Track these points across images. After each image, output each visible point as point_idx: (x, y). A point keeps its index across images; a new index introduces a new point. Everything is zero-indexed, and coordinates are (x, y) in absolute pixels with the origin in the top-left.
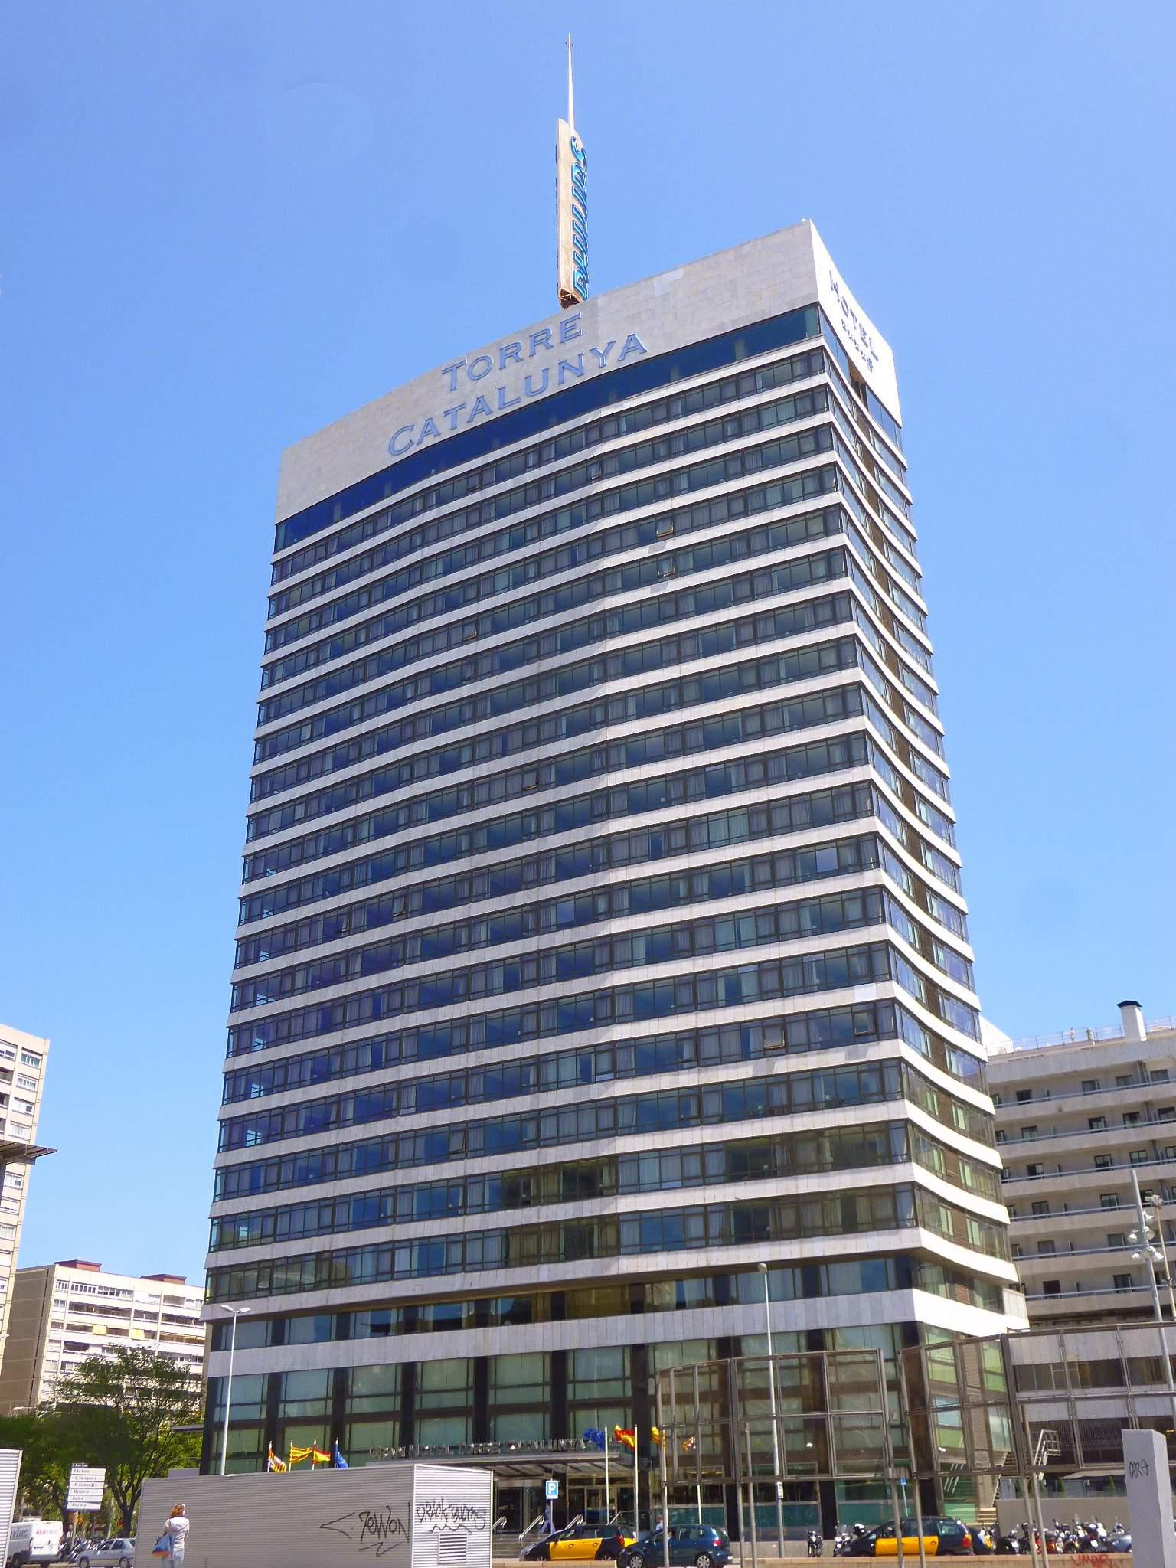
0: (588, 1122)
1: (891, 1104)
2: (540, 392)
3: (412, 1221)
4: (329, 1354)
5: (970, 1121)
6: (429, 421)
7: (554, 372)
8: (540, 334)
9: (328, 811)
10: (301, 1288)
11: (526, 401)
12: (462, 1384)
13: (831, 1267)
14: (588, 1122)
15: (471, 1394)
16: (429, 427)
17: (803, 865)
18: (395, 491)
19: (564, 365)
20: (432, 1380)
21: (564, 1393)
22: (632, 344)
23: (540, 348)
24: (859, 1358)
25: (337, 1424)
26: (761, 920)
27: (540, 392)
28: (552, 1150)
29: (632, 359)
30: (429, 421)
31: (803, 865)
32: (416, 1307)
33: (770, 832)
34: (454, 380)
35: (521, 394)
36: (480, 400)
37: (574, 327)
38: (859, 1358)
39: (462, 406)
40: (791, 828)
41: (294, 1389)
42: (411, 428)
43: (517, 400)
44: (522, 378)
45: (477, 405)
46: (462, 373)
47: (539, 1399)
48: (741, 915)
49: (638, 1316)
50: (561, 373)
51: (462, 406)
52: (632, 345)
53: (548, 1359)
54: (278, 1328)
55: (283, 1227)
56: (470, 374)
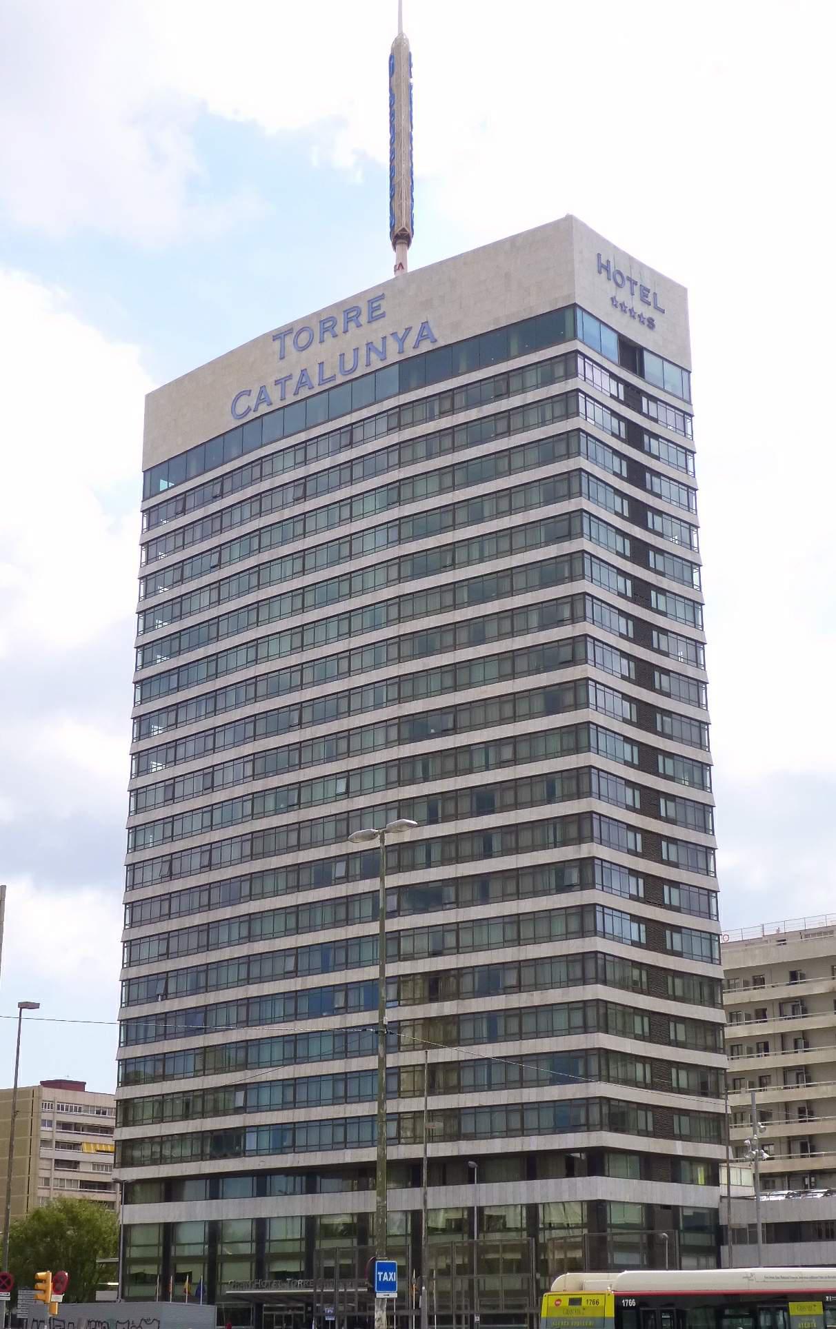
2: (353, 370)
3: (414, 1096)
4: (303, 1205)
6: (263, 390)
7: (363, 352)
8: (328, 320)
9: (538, 671)
10: (182, 1160)
12: (156, 1242)
13: (227, 1180)
15: (304, 1243)
19: (370, 346)
20: (616, 1217)
21: (264, 1247)
23: (327, 335)
27: (353, 370)
28: (354, 1061)
29: (426, 347)
30: (263, 390)
34: (283, 348)
35: (337, 371)
36: (304, 372)
37: (379, 307)
39: (290, 377)
41: (185, 1235)
42: (249, 393)
43: (333, 378)
45: (301, 378)
46: (289, 341)
47: (297, 1250)
50: (368, 356)
51: (290, 377)
52: (425, 332)
53: (585, 1206)
54: (170, 1189)
56: (295, 343)
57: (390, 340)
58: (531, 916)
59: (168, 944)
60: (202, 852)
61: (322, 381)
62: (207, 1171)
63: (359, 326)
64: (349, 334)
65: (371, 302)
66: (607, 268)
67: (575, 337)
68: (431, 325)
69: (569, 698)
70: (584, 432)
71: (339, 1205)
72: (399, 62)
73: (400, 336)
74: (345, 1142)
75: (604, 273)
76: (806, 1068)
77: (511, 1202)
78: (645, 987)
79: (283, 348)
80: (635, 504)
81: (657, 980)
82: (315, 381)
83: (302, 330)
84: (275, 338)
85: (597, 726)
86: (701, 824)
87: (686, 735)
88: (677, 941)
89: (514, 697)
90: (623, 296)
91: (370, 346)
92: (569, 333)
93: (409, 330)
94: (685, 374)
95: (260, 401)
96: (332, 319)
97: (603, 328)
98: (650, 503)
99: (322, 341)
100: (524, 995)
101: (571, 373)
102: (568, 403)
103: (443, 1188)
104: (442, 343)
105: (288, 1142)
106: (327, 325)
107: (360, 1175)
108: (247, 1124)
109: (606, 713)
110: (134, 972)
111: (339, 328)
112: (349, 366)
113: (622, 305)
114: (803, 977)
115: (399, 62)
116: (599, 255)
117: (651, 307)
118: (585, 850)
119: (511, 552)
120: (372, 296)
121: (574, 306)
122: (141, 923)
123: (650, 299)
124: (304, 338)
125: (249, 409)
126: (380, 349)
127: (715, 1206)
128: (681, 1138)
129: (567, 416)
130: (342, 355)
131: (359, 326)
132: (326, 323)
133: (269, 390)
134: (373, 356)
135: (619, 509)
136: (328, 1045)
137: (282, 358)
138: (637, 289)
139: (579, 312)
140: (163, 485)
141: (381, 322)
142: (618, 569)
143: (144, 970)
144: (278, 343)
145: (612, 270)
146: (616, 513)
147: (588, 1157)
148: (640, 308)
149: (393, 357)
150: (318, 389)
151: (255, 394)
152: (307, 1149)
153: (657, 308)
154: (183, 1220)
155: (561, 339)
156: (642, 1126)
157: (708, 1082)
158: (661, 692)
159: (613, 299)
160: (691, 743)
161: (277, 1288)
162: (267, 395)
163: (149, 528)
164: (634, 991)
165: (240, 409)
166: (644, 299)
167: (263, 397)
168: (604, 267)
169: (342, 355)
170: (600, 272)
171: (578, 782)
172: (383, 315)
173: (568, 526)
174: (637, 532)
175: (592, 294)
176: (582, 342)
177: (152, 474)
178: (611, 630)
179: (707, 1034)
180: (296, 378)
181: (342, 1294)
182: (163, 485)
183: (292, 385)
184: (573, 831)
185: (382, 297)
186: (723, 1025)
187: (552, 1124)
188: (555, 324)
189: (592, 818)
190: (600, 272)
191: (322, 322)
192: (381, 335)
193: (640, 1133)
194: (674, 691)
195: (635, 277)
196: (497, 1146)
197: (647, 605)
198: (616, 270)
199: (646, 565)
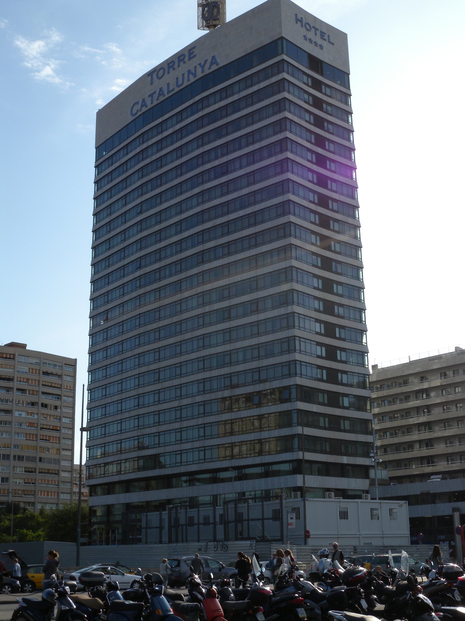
2: (182, 84)
5: (314, 101)
6: (144, 100)
7: (186, 75)
11: (177, 90)
16: (144, 104)
18: (214, 86)
19: (189, 72)
24: (295, 537)
29: (214, 68)
30: (144, 100)
32: (239, 399)
34: (152, 79)
36: (161, 89)
37: (193, 53)
38: (295, 537)
39: (155, 93)
42: (137, 103)
43: (173, 90)
46: (155, 75)
51: (155, 93)
56: (157, 76)
63: (184, 63)
64: (180, 67)
65: (190, 50)
66: (301, 21)
73: (202, 64)
76: (432, 457)
79: (152, 79)
80: (317, 117)
82: (166, 92)
83: (160, 69)
90: (311, 35)
91: (189, 72)
92: (280, 51)
93: (206, 61)
95: (142, 106)
97: (298, 49)
98: (334, 258)
99: (168, 73)
101: (291, 350)
102: (289, 320)
104: (221, 65)
106: (171, 65)
111: (176, 66)
112: (180, 83)
114: (426, 379)
116: (296, 15)
117: (327, 42)
118: (289, 309)
119: (253, 123)
120: (189, 48)
121: (282, 38)
123: (326, 37)
124: (161, 72)
125: (138, 111)
126: (194, 72)
129: (288, 328)
130: (177, 78)
133: (146, 100)
134: (191, 76)
137: (152, 84)
138: (318, 33)
141: (194, 59)
144: (150, 97)
145: (304, 22)
148: (320, 41)
149: (200, 75)
150: (167, 96)
153: (329, 42)
158: (339, 316)
159: (305, 37)
165: (134, 112)
167: (144, 104)
169: (177, 78)
170: (297, 23)
174: (319, 150)
178: (309, 308)
180: (157, 93)
183: (156, 96)
185: (194, 47)
188: (276, 46)
190: (297, 23)
191: (169, 64)
192: (194, 65)
193: (320, 404)
195: (317, 27)
199: (332, 292)
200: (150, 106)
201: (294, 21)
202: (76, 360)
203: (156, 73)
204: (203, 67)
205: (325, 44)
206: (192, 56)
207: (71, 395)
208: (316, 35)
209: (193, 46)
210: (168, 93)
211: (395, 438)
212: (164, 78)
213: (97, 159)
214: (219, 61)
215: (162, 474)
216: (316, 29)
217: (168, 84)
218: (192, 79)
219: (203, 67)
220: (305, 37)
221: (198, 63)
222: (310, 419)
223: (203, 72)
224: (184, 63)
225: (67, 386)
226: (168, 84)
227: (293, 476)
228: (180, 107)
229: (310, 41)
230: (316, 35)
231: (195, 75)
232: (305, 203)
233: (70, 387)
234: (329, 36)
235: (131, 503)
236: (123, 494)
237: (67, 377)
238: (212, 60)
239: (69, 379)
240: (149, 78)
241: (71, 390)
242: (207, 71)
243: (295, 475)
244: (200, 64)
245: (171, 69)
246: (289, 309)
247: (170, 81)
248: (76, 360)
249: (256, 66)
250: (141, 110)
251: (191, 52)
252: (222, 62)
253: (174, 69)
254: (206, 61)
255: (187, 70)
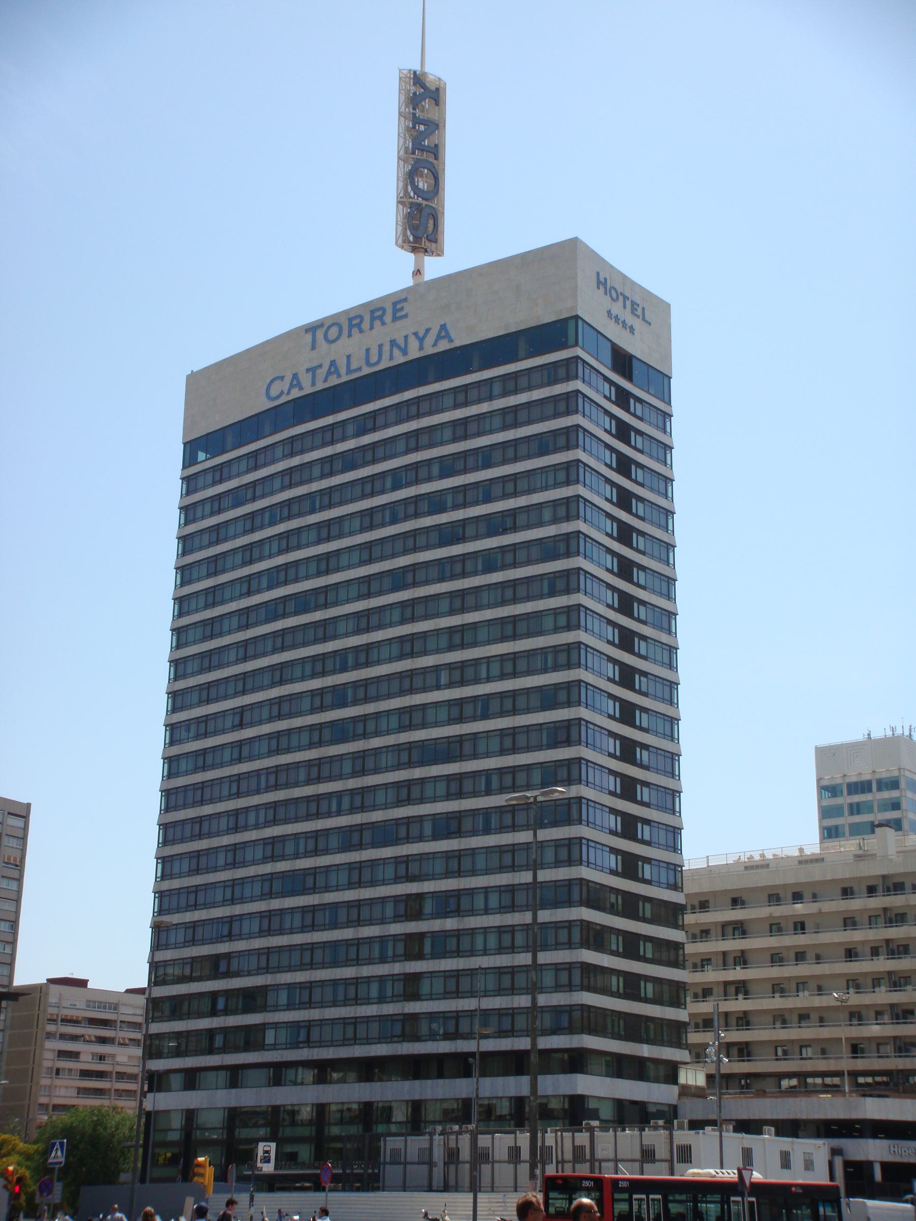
0: (399, 545)
1: (574, 868)
2: (377, 363)
6: (295, 376)
7: (387, 348)
8: (355, 317)
11: (366, 371)
14: (399, 545)
17: (532, 624)
19: (393, 343)
22: (443, 334)
25: (235, 1156)
26: (503, 894)
29: (444, 346)
30: (295, 376)
31: (532, 624)
33: (514, 750)
35: (363, 363)
36: (333, 363)
37: (402, 309)
39: (320, 366)
40: (529, 562)
43: (359, 369)
44: (365, 348)
48: (491, 1012)
49: (417, 1081)
51: (320, 366)
55: (211, 728)
57: (412, 339)
58: (525, 729)
59: (198, 862)
60: (234, 714)
61: (349, 371)
62: (229, 1063)
64: (374, 331)
67: (576, 344)
68: (449, 327)
69: (562, 696)
70: (581, 427)
71: (349, 1093)
72: (423, 101)
73: (421, 335)
74: (355, 1038)
75: (601, 287)
77: (500, 1095)
78: (620, 908)
81: (630, 906)
82: (343, 370)
84: (307, 331)
85: (588, 800)
86: (670, 770)
87: (657, 588)
88: (643, 647)
89: (516, 442)
90: (617, 309)
91: (393, 343)
92: (571, 340)
93: (428, 331)
94: (666, 379)
95: (292, 386)
96: (361, 317)
99: (350, 335)
100: (517, 914)
103: (441, 1081)
104: (458, 343)
105: (302, 1037)
107: (368, 1069)
108: (267, 1021)
109: (598, 755)
110: (166, 885)
111: (366, 325)
113: (616, 318)
115: (423, 101)
116: (598, 274)
118: (574, 791)
121: (577, 318)
122: (176, 808)
123: (639, 312)
125: (282, 393)
126: (403, 346)
127: (675, 1103)
128: (648, 1041)
130: (368, 350)
131: (383, 324)
132: (353, 321)
134: (396, 352)
135: (608, 427)
136: (356, 523)
138: (628, 303)
139: (580, 323)
140: (201, 456)
142: (609, 731)
143: (176, 884)
144: (310, 374)
145: (608, 287)
146: (607, 499)
147: (570, 1057)
148: (630, 320)
149: (414, 353)
150: (345, 378)
151: (288, 380)
152: (321, 1044)
153: (644, 319)
154: (204, 1106)
155: (564, 346)
156: (614, 947)
157: (674, 994)
159: (609, 312)
160: (661, 594)
161: (290, 1168)
162: (299, 382)
163: (186, 524)
164: (611, 913)
165: (274, 392)
166: (633, 311)
168: (601, 283)
169: (368, 350)
170: (598, 288)
171: (569, 656)
172: (406, 316)
173: (565, 734)
175: (593, 309)
176: (583, 349)
177: (191, 448)
179: (670, 953)
181: (349, 1174)
182: (201, 456)
184: (562, 406)
185: (405, 300)
186: (683, 944)
187: (539, 704)
188: (557, 333)
189: (578, 537)
190: (598, 288)
191: (350, 320)
192: (405, 333)
194: (649, 585)
195: (627, 294)
196: (490, 1045)
197: (629, 579)
198: (611, 284)
200: (308, 390)
201: (595, 284)
202: (29, 805)
203: (325, 328)
204: (421, 340)
205: (637, 323)
206: (399, 315)
207: (15, 874)
208: (625, 307)
209: (403, 297)
210: (347, 374)
211: (701, 1004)
212: (339, 342)
213: (187, 463)
214: (453, 335)
215: (315, 1057)
216: (626, 298)
217: (349, 357)
218: (400, 359)
219: (421, 340)
220: (609, 312)
221: (413, 330)
222: (591, 977)
223: (421, 348)
224: (383, 324)
225: (9, 858)
226: (349, 357)
227: (569, 1075)
228: (372, 404)
229: (617, 319)
230: (625, 307)
231: (405, 352)
232: (601, 609)
233: (15, 859)
234: (643, 309)
235: (241, 1108)
236: (225, 1091)
237: (11, 839)
238: (440, 332)
239: (13, 843)
240: (309, 337)
241: (17, 866)
242: (429, 350)
243: (574, 1075)
244: (416, 334)
245: (355, 331)
246: (574, 791)
247: (357, 356)
248: (29, 805)
249: (522, 359)
250: (288, 393)
251: (399, 307)
252: (461, 339)
253: (361, 331)
254: (428, 331)
255: (389, 339)
